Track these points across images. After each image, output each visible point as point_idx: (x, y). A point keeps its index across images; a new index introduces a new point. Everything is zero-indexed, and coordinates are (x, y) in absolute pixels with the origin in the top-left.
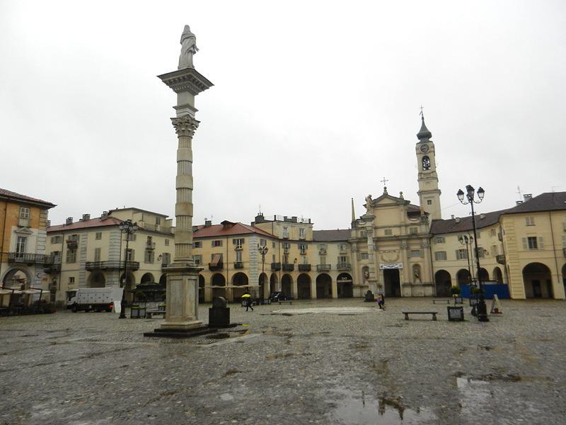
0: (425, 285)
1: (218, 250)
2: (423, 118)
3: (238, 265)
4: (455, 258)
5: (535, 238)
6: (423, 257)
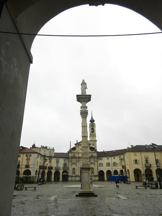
0: (95, 176)
3: (27, 166)
4: (106, 166)
5: (137, 160)
6: (95, 165)
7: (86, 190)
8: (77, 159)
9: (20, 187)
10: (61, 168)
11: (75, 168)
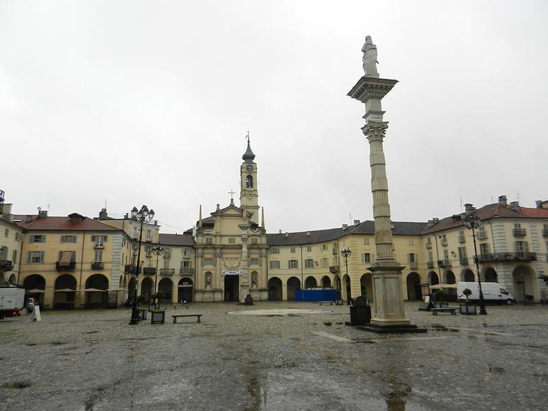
0: (261, 290)
1: (68, 247)
2: (249, 142)
3: (97, 266)
5: (369, 254)
7: (397, 319)
8: (218, 251)
9: (162, 314)
10: (177, 272)
11: (212, 271)
